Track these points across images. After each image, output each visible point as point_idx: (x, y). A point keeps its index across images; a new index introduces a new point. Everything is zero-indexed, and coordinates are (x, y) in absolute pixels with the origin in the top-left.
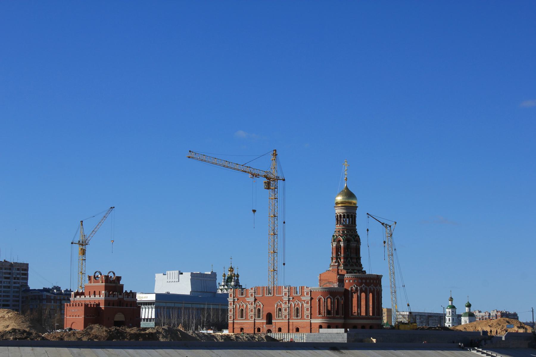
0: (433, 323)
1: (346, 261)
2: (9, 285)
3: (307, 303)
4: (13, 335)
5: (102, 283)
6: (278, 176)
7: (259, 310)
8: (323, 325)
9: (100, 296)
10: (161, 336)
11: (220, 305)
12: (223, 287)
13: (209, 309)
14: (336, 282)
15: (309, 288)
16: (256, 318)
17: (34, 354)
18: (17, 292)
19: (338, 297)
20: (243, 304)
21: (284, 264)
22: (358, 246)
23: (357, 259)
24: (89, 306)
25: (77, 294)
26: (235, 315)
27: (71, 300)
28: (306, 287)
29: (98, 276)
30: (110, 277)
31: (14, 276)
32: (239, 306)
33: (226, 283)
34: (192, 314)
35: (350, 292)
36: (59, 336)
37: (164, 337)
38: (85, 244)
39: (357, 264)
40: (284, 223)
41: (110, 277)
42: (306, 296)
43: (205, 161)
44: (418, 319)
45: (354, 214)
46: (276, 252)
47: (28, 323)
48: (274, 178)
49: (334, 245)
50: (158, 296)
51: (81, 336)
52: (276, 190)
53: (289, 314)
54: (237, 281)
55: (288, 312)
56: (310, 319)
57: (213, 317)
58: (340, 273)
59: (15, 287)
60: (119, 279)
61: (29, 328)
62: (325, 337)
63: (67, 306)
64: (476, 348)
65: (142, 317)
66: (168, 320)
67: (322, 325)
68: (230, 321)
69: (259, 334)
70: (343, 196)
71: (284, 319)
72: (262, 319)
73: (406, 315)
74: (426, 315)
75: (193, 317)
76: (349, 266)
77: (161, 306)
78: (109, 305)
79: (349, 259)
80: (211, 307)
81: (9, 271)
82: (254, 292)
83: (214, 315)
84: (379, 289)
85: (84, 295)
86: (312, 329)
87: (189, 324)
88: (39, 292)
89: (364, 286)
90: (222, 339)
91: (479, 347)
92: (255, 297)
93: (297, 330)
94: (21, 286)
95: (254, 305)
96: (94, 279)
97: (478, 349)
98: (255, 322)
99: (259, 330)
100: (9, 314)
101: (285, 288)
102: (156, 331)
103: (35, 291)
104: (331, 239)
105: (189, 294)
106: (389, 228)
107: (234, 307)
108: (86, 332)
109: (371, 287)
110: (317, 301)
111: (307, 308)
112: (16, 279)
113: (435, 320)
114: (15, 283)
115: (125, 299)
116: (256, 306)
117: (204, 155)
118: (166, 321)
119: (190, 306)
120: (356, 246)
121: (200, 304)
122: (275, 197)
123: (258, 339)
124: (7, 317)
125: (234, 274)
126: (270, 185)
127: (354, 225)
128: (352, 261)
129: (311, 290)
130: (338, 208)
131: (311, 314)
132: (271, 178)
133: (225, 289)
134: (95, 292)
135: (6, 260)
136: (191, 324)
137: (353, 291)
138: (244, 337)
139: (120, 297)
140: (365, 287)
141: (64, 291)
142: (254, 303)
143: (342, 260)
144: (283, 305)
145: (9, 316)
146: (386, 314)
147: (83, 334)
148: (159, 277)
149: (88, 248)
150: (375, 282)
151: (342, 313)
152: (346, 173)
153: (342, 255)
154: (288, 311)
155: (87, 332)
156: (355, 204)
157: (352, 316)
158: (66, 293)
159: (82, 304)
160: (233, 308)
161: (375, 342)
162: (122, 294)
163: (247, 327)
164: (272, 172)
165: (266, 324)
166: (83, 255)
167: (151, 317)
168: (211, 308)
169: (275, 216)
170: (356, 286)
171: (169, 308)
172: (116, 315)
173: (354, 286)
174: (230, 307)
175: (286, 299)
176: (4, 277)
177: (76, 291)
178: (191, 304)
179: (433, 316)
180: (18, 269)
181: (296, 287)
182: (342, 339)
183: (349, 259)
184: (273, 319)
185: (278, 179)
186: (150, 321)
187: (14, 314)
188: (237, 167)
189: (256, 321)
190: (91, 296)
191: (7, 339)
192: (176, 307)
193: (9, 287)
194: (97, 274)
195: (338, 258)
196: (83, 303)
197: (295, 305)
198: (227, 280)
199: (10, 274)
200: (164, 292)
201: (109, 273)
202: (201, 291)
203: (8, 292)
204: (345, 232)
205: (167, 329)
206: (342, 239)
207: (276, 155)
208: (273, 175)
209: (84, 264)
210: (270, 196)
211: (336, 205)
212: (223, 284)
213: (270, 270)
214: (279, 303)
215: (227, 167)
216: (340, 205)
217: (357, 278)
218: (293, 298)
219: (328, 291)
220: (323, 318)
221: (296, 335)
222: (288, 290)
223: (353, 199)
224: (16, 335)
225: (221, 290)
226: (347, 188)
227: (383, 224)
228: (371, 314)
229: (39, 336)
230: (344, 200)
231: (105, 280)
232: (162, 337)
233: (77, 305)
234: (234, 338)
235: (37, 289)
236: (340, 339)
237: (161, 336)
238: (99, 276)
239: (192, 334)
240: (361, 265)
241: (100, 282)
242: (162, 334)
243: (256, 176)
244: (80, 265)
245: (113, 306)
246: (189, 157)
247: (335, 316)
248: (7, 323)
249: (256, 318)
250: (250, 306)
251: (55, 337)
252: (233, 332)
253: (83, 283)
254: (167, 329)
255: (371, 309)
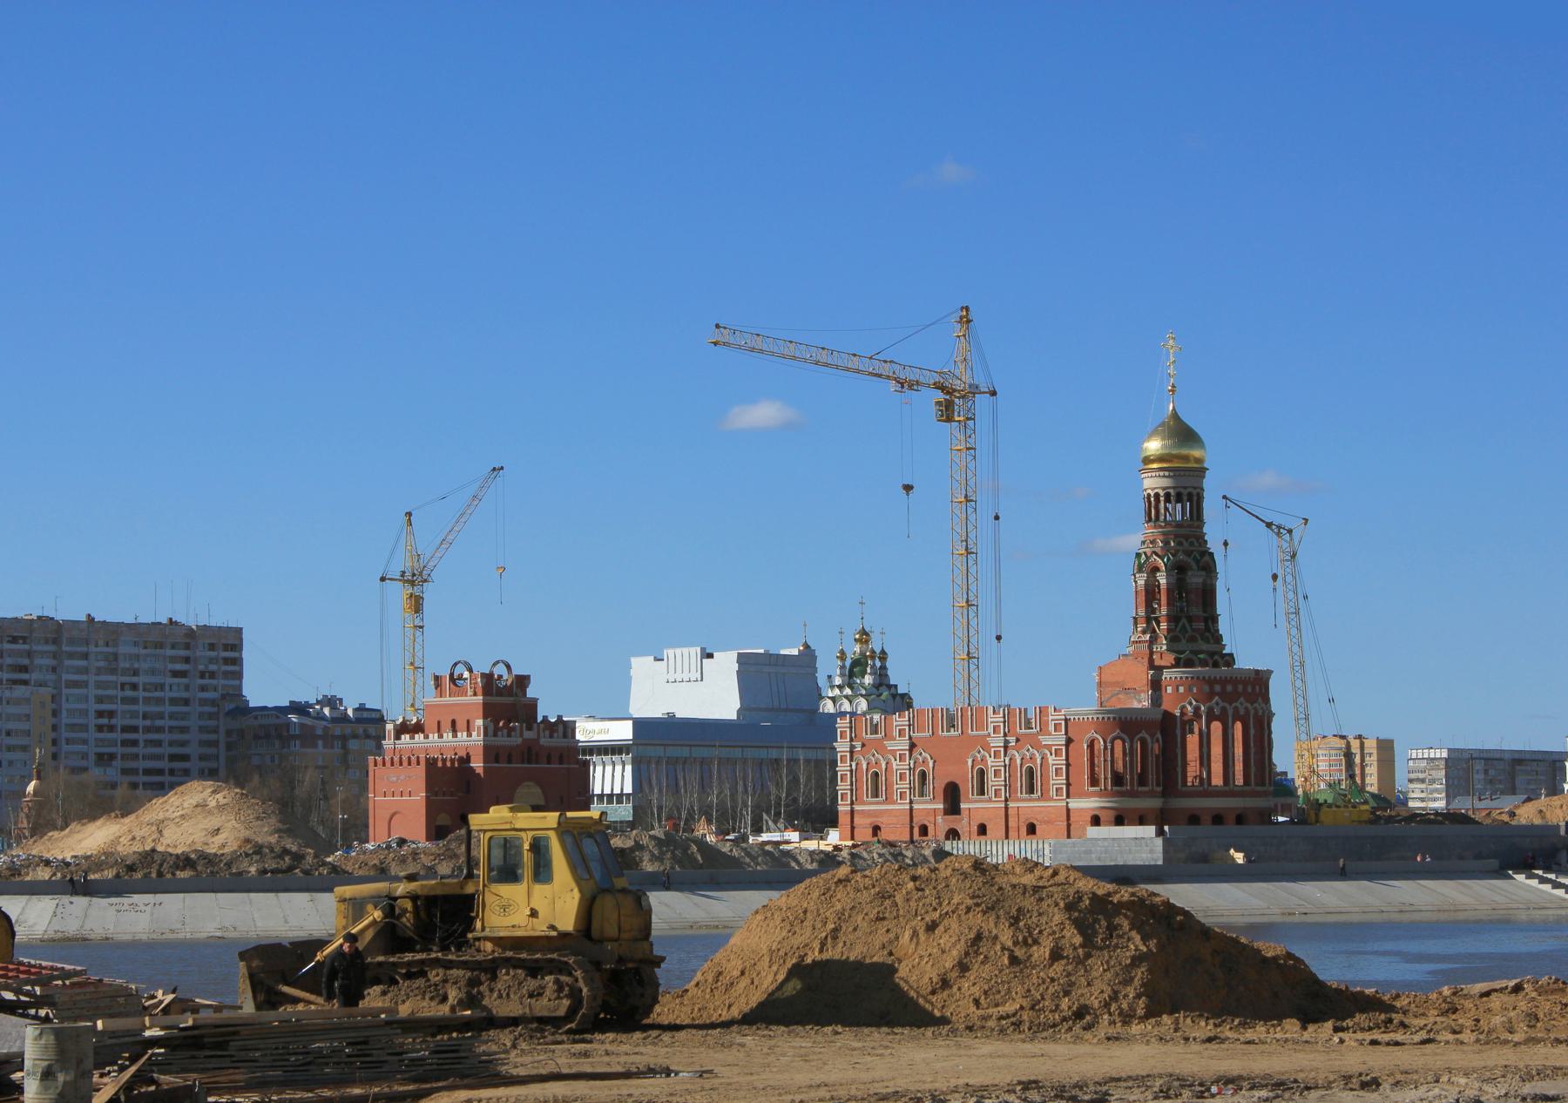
0: (1528, 783)
1: (1176, 626)
2: (184, 695)
3: (1057, 753)
4: (257, 862)
5: (475, 694)
6: (976, 382)
7: (923, 775)
8: (1103, 816)
9: (469, 735)
10: (646, 857)
11: (827, 750)
12: (839, 693)
13: (793, 762)
14: (1146, 689)
15: (1061, 711)
16: (914, 796)
17: (318, 911)
18: (211, 716)
19: (1144, 734)
20: (878, 759)
21: (999, 638)
22: (1209, 582)
23: (1206, 620)
24: (440, 764)
25: (403, 729)
26: (856, 789)
27: (385, 747)
28: (1053, 709)
29: (462, 675)
30: (496, 676)
31: (201, 667)
32: (868, 764)
33: (847, 678)
34: (745, 779)
35: (1178, 720)
36: (376, 862)
37: (653, 858)
38: (420, 579)
39: (1207, 634)
40: (997, 518)
41: (496, 676)
42: (1053, 733)
43: (761, 351)
44: (1478, 773)
45: (1198, 490)
46: (974, 605)
47: (273, 820)
48: (962, 391)
49: (1141, 582)
50: (641, 725)
51: (435, 860)
52: (970, 423)
53: (1008, 785)
54: (884, 672)
55: (1005, 781)
56: (1065, 797)
57: (806, 786)
58: (1158, 662)
59: (203, 702)
60: (523, 681)
61: (276, 835)
62: (1103, 849)
63: (376, 765)
64: (1540, 872)
65: (593, 790)
66: (671, 801)
67: (1100, 816)
68: (843, 808)
69: (923, 842)
70: (1163, 439)
71: (994, 799)
72: (931, 802)
73: (1441, 758)
74: (1507, 756)
75: (745, 786)
76: (1184, 641)
77: (650, 757)
78: (497, 762)
79: (1184, 621)
80: (801, 755)
81: (183, 653)
82: (907, 723)
83: (809, 779)
84: (1262, 708)
85: (423, 732)
86: (1072, 828)
87: (734, 808)
88: (279, 714)
89: (1217, 704)
90: (812, 862)
91: (1548, 869)
92: (910, 738)
93: (1032, 829)
94: (224, 697)
95: (910, 759)
96: (452, 685)
97: (1545, 875)
98: (911, 810)
99: (924, 830)
100: (217, 796)
101: (994, 712)
102: (633, 843)
103: (266, 713)
104: (1131, 563)
105: (734, 716)
106: (1287, 537)
107: (854, 767)
108: (447, 850)
109: (1238, 704)
110: (1086, 747)
111: (1056, 769)
112: (207, 675)
113: (1537, 772)
114: (203, 689)
115: (543, 741)
116: (915, 763)
117: (758, 335)
118: (667, 802)
119: (737, 753)
120: (1204, 584)
121: (767, 747)
122: (968, 445)
123: (912, 859)
124: (213, 804)
125: (873, 651)
126: (953, 411)
127: (1196, 524)
128: (1191, 626)
129: (1068, 717)
130: (1150, 475)
131: (1068, 785)
132: (955, 390)
133: (847, 697)
134: (454, 723)
135: (174, 620)
136: (741, 810)
137: (1186, 718)
138: (875, 854)
139: (528, 735)
140: (1220, 706)
141: (355, 710)
142: (907, 755)
143: (1164, 626)
144: (990, 761)
145: (218, 801)
146: (1375, 757)
147: (439, 855)
148: (641, 666)
149: (430, 593)
150: (1250, 690)
151: (1158, 779)
152: (1171, 371)
153: (1164, 610)
154: (1005, 778)
155: (449, 849)
156: (1199, 461)
157: (1184, 789)
158: (359, 715)
159: (418, 758)
160: (851, 771)
161: (1240, 861)
162: (535, 725)
163: (890, 822)
164: (957, 372)
165: (945, 814)
166: (417, 612)
167: (622, 789)
168: (799, 760)
169: (967, 499)
170: (1194, 703)
171: (673, 762)
172: (518, 791)
173: (1191, 704)
174: (842, 768)
175: (997, 742)
176: (170, 671)
177: (401, 720)
178: (739, 747)
179: (1529, 760)
180: (212, 647)
181: (1026, 710)
182: (1149, 855)
183: (1184, 621)
184: (962, 798)
185: (974, 390)
186: (620, 801)
187: (233, 794)
188: (855, 363)
189: (915, 806)
190: (445, 735)
191: (240, 874)
192: (695, 759)
193: (186, 702)
194: (460, 669)
195: (1150, 618)
196: (422, 756)
197: (1022, 759)
198: (851, 671)
199: (187, 660)
200: (655, 711)
201: (495, 664)
202: (771, 707)
203: (184, 716)
204: (1172, 544)
205: (663, 837)
206: (1162, 564)
207: (969, 321)
208: (960, 380)
209: (419, 640)
210: (955, 442)
211: (1145, 464)
212: (838, 681)
213: (959, 657)
214: (977, 754)
215: (826, 365)
216: (1155, 466)
217: (1197, 679)
218: (1018, 740)
219: (1114, 718)
220: (1100, 794)
221: (1023, 846)
222: (1004, 717)
223: (1191, 447)
224: (263, 861)
225: (833, 699)
226: (1175, 415)
227: (1269, 525)
228: (1239, 781)
229: (324, 864)
230: (1167, 452)
231: (484, 688)
232: (651, 860)
233: (405, 763)
234: (845, 858)
235: (270, 706)
236: (1144, 855)
237: (646, 857)
238: (465, 676)
239: (731, 851)
240: (1218, 639)
241: (470, 692)
242: (650, 851)
243: (911, 387)
244: (407, 643)
245: (509, 762)
246: (715, 344)
247: (1136, 788)
248: (214, 822)
249: (914, 796)
250: (897, 765)
251: (366, 864)
252: (852, 838)
253: (419, 696)
254: (663, 837)
255: (1239, 767)
